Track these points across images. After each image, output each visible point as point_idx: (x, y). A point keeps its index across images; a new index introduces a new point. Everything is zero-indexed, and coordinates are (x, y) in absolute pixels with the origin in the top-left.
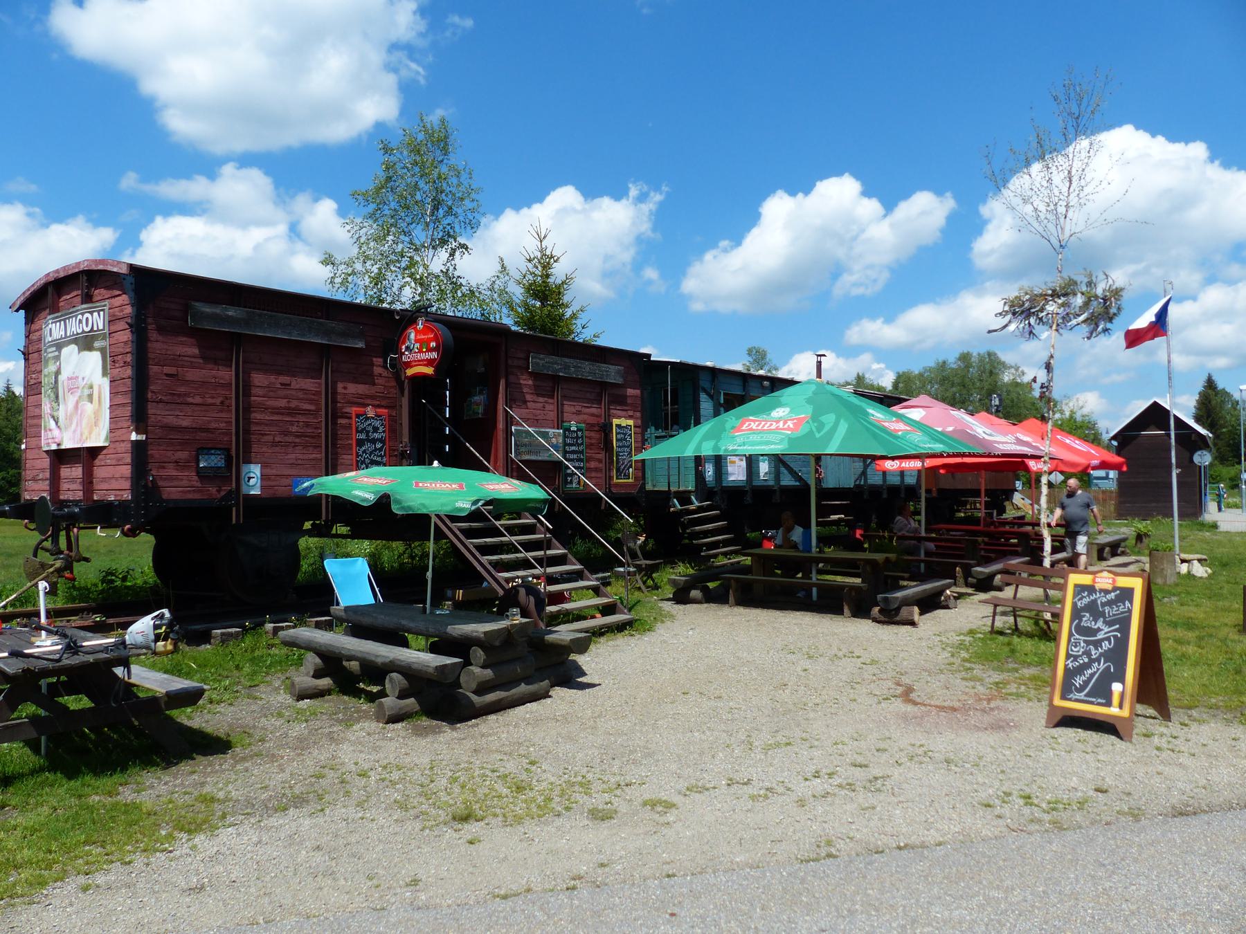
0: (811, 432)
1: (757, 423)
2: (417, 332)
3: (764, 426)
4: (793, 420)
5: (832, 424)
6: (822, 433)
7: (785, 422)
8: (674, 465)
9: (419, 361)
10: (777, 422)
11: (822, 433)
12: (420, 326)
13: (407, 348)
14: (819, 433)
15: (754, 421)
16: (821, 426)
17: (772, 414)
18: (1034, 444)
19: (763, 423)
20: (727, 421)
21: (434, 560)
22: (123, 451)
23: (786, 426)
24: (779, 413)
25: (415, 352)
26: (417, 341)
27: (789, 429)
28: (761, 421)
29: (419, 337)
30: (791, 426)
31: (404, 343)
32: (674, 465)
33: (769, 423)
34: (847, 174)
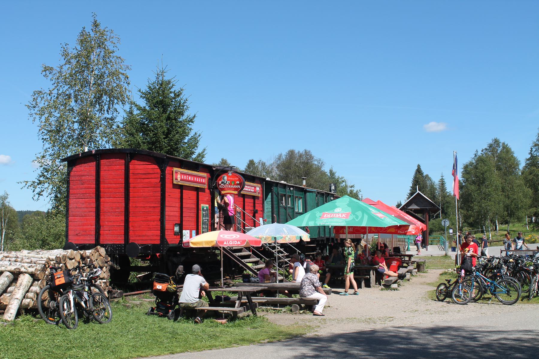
0: (354, 219)
1: (330, 215)
2: (228, 176)
3: (333, 216)
4: (345, 214)
5: (361, 216)
6: (358, 220)
7: (342, 214)
8: (322, 230)
9: (230, 188)
10: (339, 214)
11: (358, 220)
12: (230, 174)
13: (222, 183)
14: (357, 219)
15: (329, 214)
16: (357, 217)
17: (335, 211)
18: (452, 352)
19: (332, 215)
20: (316, 213)
21: (369, 230)
22: (77, 225)
23: (343, 217)
24: (337, 210)
25: (227, 185)
26: (228, 180)
27: (344, 217)
28: (331, 214)
29: (229, 179)
30: (345, 216)
31: (220, 180)
32: (322, 230)
33: (335, 214)
34: (413, 204)
